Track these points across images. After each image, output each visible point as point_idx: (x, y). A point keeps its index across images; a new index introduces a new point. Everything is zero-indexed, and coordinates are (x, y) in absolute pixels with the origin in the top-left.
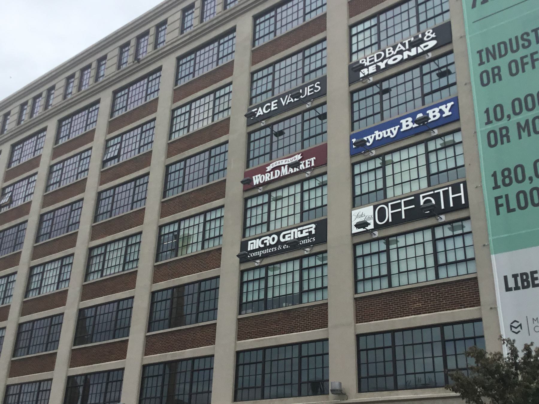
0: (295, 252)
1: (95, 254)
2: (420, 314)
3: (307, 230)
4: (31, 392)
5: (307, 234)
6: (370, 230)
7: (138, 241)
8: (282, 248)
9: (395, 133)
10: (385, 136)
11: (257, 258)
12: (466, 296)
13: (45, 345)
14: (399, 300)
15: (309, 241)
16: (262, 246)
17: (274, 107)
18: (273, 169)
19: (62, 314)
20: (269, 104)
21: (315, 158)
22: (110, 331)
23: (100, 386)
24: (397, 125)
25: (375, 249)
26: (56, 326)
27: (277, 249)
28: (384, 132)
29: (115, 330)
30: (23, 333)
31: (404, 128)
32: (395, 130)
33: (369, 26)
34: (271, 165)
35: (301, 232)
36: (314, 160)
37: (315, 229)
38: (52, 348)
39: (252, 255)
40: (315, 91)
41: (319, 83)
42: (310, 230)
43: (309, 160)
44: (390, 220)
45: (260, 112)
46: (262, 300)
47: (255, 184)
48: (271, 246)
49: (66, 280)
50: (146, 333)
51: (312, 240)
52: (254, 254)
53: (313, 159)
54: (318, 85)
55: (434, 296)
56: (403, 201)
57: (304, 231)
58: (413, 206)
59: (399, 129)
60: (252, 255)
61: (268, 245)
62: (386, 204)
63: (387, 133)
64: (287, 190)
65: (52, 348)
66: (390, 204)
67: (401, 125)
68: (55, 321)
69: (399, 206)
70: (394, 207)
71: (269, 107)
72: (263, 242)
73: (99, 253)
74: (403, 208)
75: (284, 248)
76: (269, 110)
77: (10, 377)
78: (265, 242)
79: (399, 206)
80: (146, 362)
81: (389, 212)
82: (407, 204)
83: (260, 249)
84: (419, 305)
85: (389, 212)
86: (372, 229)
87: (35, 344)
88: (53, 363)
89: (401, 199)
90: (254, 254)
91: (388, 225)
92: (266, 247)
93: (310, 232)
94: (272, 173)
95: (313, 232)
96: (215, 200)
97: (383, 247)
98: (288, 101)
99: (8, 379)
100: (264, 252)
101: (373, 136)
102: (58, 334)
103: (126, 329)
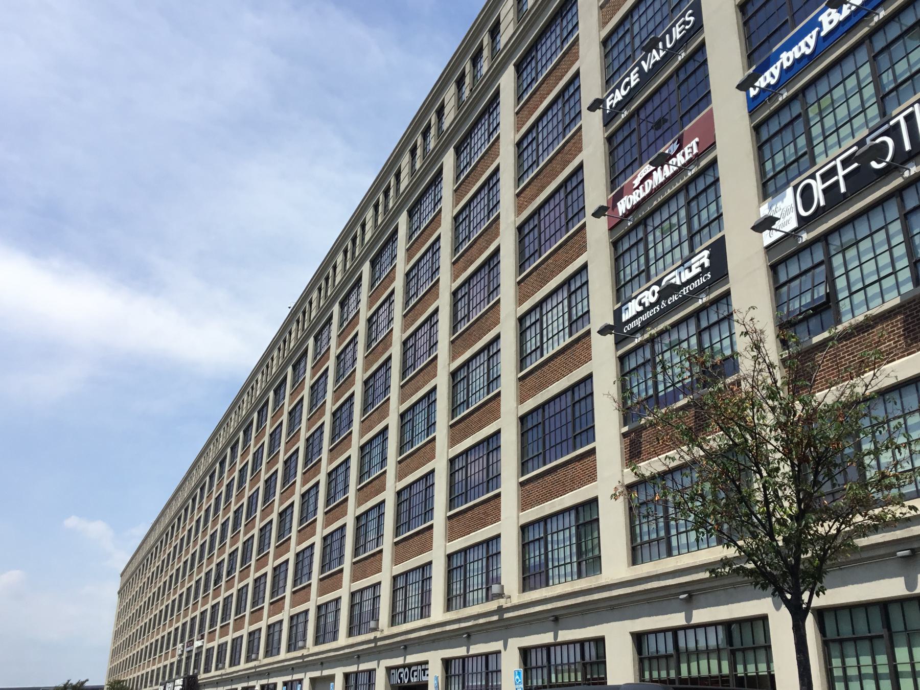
0: (874, 192)
1: (528, 324)
2: (894, 360)
3: (698, 264)
4: (478, 560)
5: (699, 270)
6: (792, 231)
7: (584, 280)
8: (667, 303)
9: (812, 43)
10: (798, 55)
11: (636, 331)
12: (173, 656)
13: (485, 485)
14: (855, 344)
15: (702, 280)
16: (640, 309)
17: (635, 80)
18: (642, 182)
19: (590, 377)
20: (627, 80)
21: (697, 140)
22: (483, 483)
23: (567, 532)
24: (813, 29)
25: (806, 264)
26: (583, 403)
27: (660, 307)
28: (795, 49)
29: (488, 482)
30: (457, 473)
31: (827, 28)
32: (811, 39)
33: (777, 128)
34: (639, 176)
35: (690, 269)
36: (697, 143)
37: (709, 258)
38: (553, 457)
39: (692, 286)
40: (687, 27)
41: (690, 12)
42: (701, 262)
43: (689, 146)
44: (822, 203)
45: (654, 57)
46: (651, 396)
47: (621, 214)
48: (652, 305)
49: (582, 316)
50: (518, 478)
51: (707, 277)
52: (632, 325)
53: (693, 143)
54: (690, 15)
55: (914, 322)
56: (839, 160)
57: (693, 267)
58: (856, 165)
59: (819, 33)
60: (692, 286)
61: (647, 305)
62: (813, 177)
63: (800, 49)
64: (814, 91)
65: (553, 457)
66: (818, 175)
67: (820, 25)
68: (581, 393)
69: (833, 172)
70: (825, 178)
71: (628, 83)
72: (640, 304)
73: (641, 361)
74: (841, 173)
75: (669, 303)
76: (629, 87)
77: (523, 510)
78: (642, 302)
79: (833, 172)
80: (523, 521)
81: (818, 187)
82: (845, 163)
83: (639, 314)
84: (890, 345)
85: (818, 187)
86: (795, 230)
87: (553, 444)
88: (498, 509)
89: (835, 159)
90: (632, 325)
91: (821, 214)
92: (646, 309)
93: (702, 266)
94: (641, 187)
95: (707, 265)
96: (578, 257)
97: (819, 256)
98: (652, 62)
99: (448, 544)
100: (643, 318)
101: (778, 64)
102: (590, 414)
103: (589, 433)
